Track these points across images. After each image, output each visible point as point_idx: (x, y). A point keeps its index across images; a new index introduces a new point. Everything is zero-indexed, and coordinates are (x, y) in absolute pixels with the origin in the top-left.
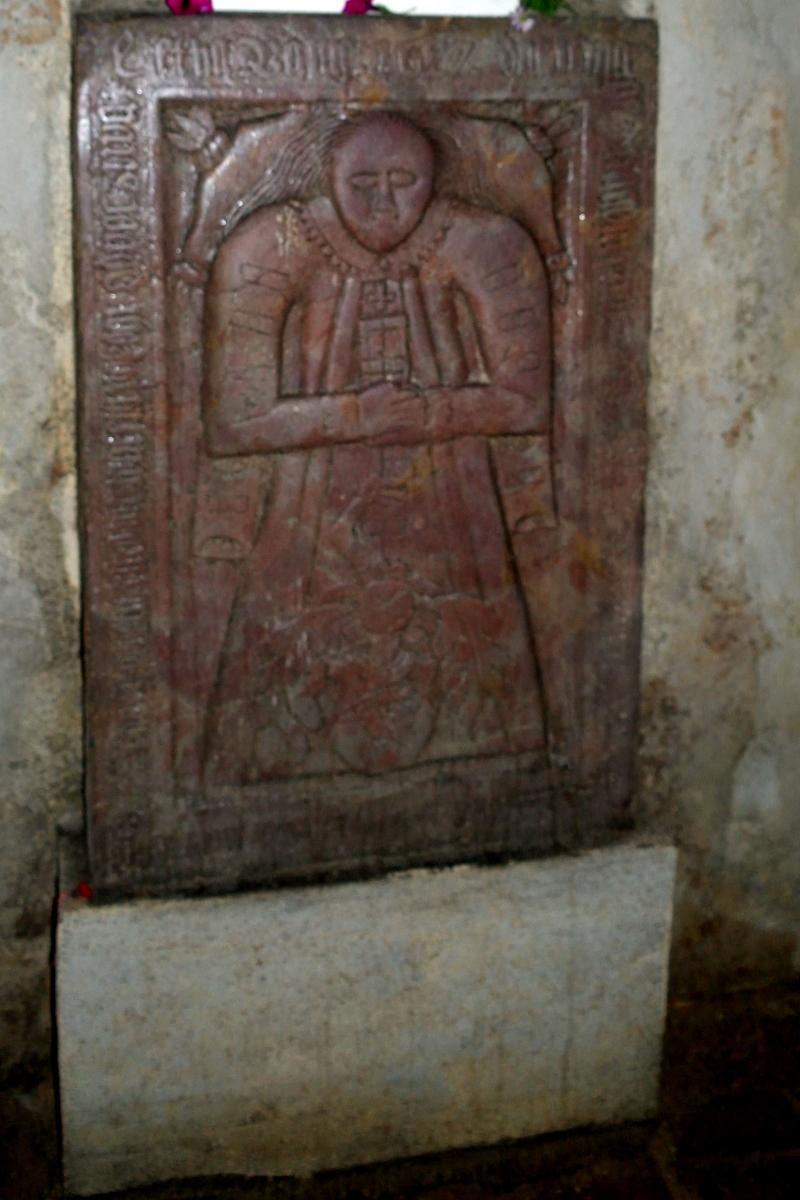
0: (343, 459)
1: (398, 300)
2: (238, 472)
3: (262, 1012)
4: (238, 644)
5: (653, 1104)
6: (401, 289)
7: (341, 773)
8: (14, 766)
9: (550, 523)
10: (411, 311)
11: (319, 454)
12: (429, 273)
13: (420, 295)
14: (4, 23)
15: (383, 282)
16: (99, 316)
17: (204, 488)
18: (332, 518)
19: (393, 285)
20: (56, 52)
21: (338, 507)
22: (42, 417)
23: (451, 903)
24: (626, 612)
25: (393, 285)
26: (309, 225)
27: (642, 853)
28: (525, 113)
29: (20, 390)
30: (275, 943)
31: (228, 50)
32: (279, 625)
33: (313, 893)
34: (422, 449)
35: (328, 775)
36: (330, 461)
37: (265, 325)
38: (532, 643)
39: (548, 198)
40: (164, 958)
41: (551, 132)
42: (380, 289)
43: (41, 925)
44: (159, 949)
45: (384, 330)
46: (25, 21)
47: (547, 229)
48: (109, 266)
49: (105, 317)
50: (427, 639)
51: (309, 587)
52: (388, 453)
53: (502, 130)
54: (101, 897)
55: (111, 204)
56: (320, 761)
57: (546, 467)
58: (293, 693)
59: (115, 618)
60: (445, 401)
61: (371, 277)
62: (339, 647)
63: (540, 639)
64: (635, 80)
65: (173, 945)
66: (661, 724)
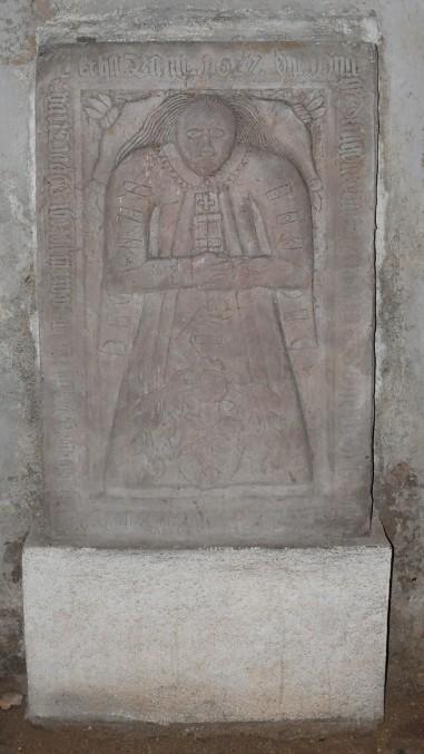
1: (217, 204)
3: (137, 621)
5: (380, 710)
7: (184, 487)
8: (10, 479)
9: (311, 343)
10: (224, 210)
13: (230, 203)
14: (6, 54)
15: (207, 193)
19: (213, 196)
20: (32, 67)
22: (25, 275)
23: (249, 569)
27: (369, 550)
28: (293, 97)
29: (14, 259)
30: (144, 581)
31: (119, 61)
33: (166, 554)
34: (232, 293)
37: (139, 217)
38: (302, 416)
39: (307, 146)
40: (82, 582)
41: (308, 108)
42: (206, 198)
43: (15, 550)
44: (78, 576)
45: (208, 222)
46: (17, 52)
47: (307, 165)
53: (279, 106)
54: (47, 541)
55: (54, 148)
57: (310, 309)
63: (307, 416)
65: (86, 575)
66: (406, 493)
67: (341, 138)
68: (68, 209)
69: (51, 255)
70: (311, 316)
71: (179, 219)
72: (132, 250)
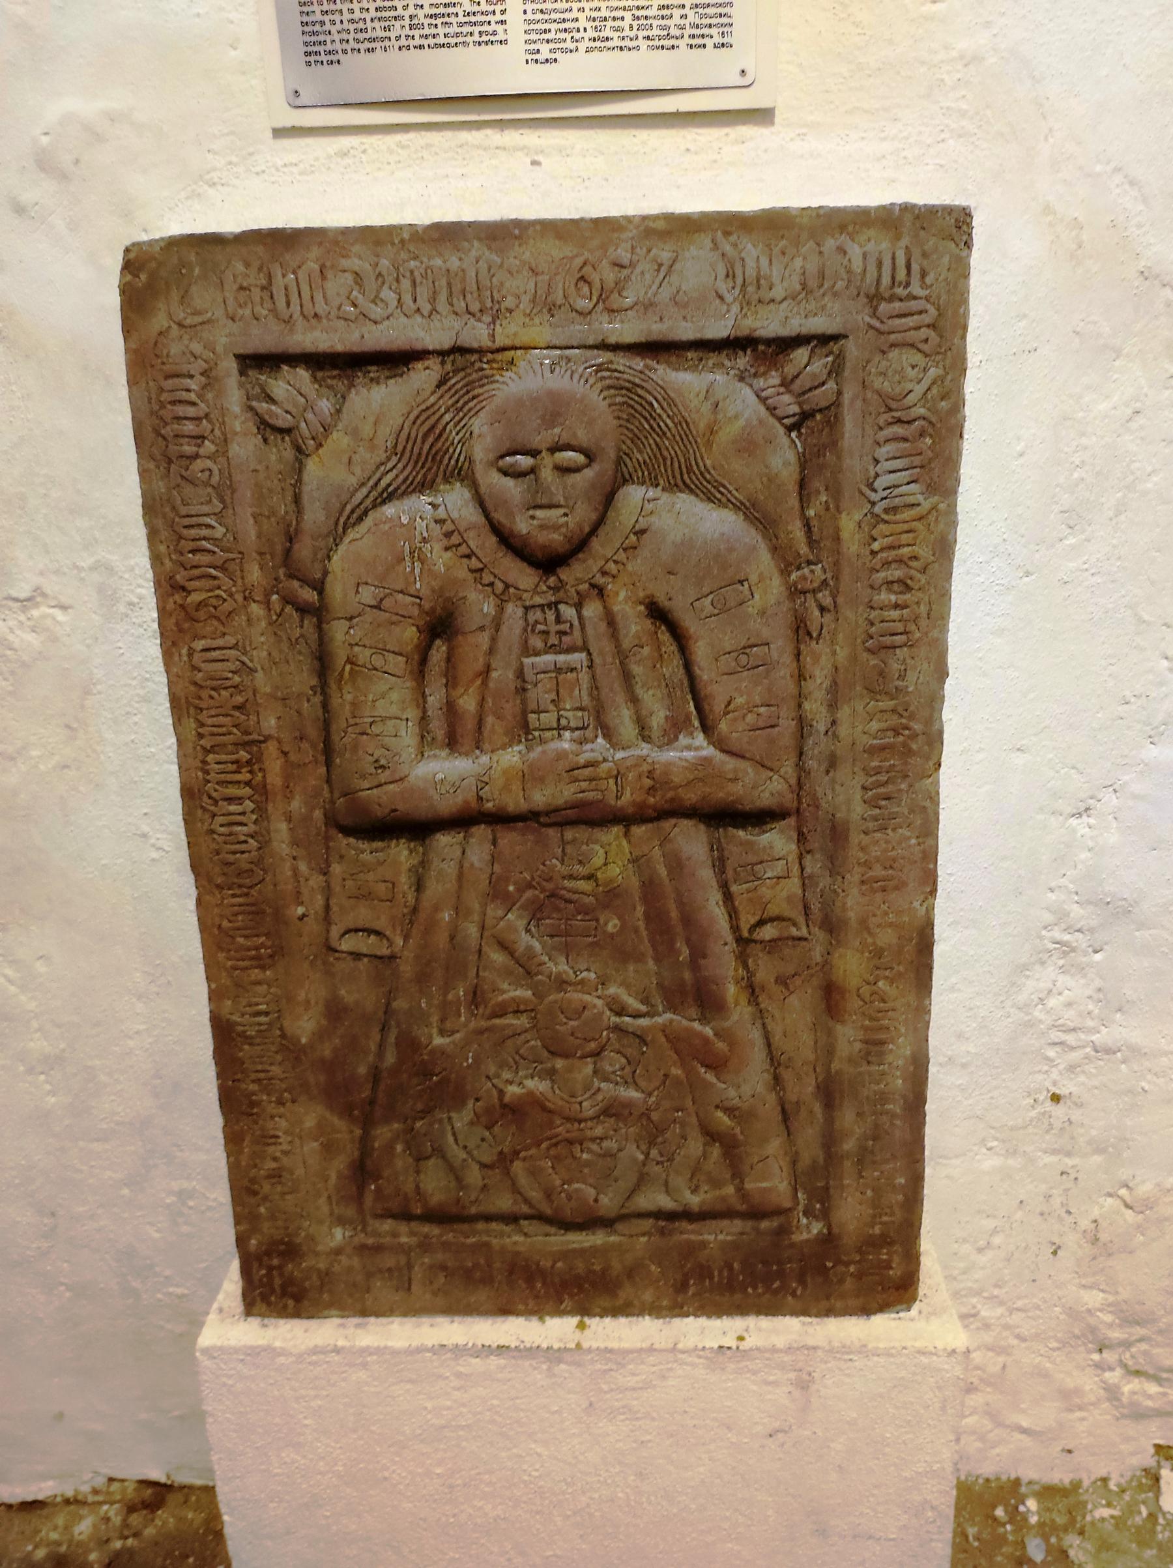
0: (509, 839)
1: (577, 632)
2: (480, 1413)
4: (390, 1058)
6: (580, 617)
7: (527, 1217)
11: (481, 832)
12: (617, 594)
16: (184, 651)
17: (336, 869)
18: (500, 913)
19: (568, 612)
21: (509, 902)
24: (900, 1051)
25: (568, 612)
26: (449, 526)
32: (438, 1041)
35: (512, 1219)
36: (494, 843)
42: (551, 616)
48: (191, 585)
49: (190, 654)
50: (628, 1069)
51: (476, 997)
52: (569, 834)
56: (504, 1202)
57: (793, 857)
58: (461, 1119)
59: (236, 1018)
60: (884, 588)
61: (538, 600)
62: (755, 1288)
64: (927, 299)
67: (877, 461)
68: (235, 647)
69: (207, 751)
70: (795, 870)
71: (488, 669)
72: (387, 741)
